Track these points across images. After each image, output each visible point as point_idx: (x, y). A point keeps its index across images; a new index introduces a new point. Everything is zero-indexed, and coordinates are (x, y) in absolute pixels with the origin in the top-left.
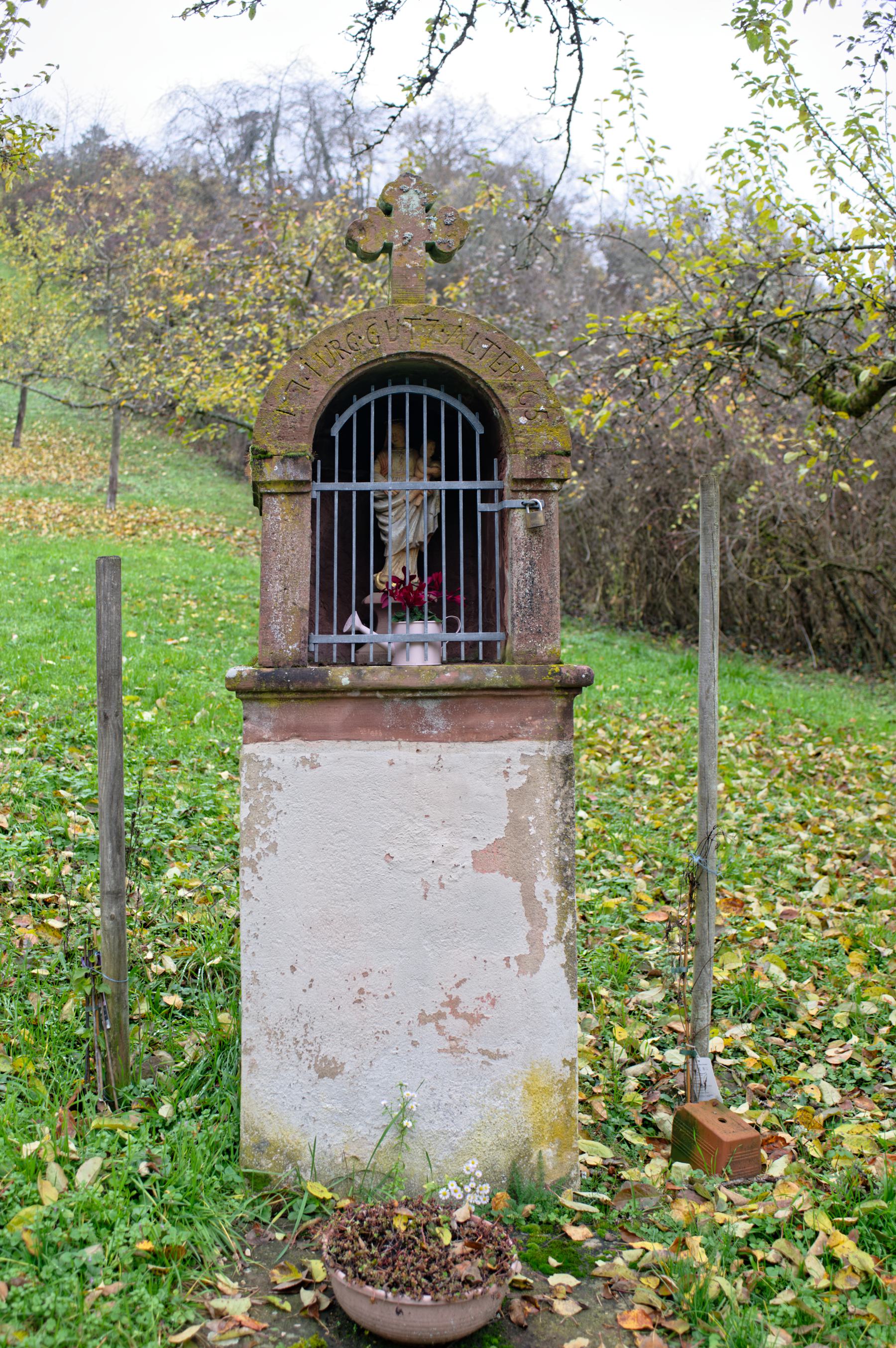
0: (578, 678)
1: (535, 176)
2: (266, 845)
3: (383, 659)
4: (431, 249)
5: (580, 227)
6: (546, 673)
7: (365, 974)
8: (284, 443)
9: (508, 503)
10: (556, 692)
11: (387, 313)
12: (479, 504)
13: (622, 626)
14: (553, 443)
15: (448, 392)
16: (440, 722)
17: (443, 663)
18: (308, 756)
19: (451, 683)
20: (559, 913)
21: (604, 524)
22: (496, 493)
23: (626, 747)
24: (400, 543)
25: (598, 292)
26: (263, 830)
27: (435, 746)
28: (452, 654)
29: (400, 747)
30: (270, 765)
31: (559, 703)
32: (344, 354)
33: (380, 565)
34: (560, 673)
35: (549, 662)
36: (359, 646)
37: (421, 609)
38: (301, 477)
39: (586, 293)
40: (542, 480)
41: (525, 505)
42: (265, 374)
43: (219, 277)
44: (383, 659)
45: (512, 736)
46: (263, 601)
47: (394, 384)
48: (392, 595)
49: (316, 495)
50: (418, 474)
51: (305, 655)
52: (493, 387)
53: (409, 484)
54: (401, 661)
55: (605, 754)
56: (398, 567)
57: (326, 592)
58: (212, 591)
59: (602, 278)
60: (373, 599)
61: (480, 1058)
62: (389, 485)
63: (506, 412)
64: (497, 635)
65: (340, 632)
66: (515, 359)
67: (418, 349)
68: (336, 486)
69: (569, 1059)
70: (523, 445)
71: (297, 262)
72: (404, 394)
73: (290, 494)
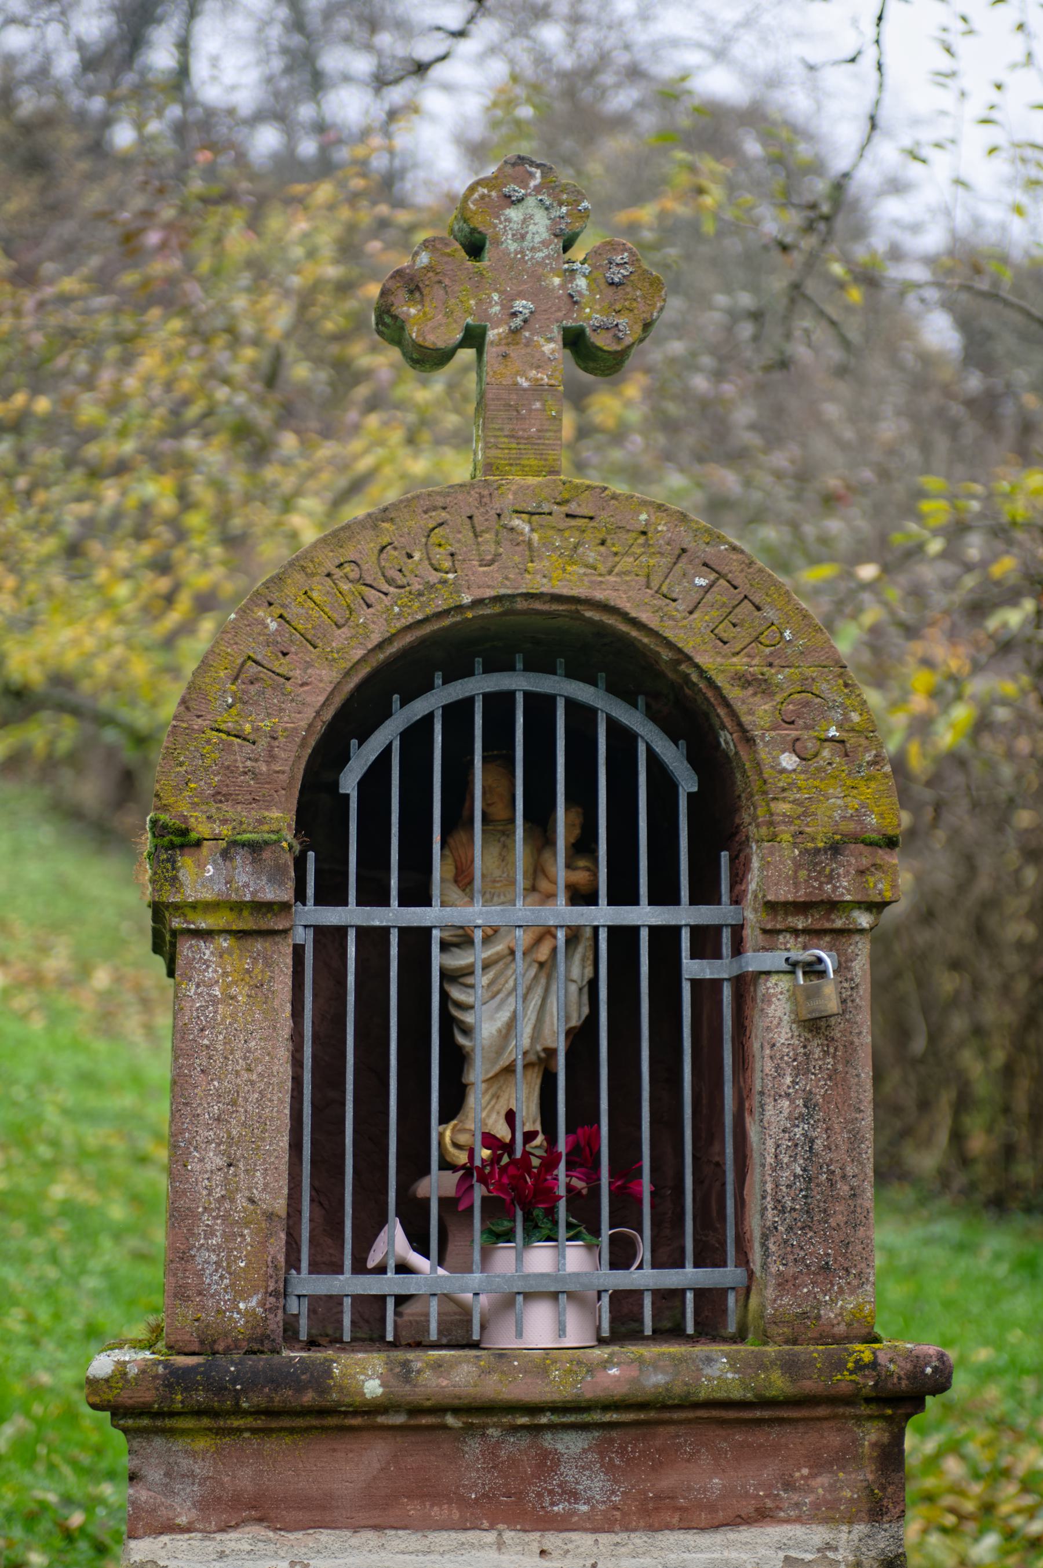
0: (915, 1374)
1: (799, 132)
3: (461, 1333)
4: (575, 341)
5: (896, 254)
6: (839, 1365)
8: (229, 810)
9: (754, 961)
10: (865, 1410)
11: (472, 498)
12: (686, 960)
13: (999, 1204)
14: (858, 816)
15: (615, 689)
16: (595, 1485)
17: (601, 1341)
19: (620, 1391)
21: (956, 965)
22: (726, 935)
23: (1009, 1498)
24: (500, 1050)
25: (940, 412)
27: (583, 1540)
28: (623, 1321)
29: (500, 1545)
31: (872, 1434)
32: (371, 595)
33: (454, 1103)
34: (874, 1364)
35: (848, 1339)
36: (401, 1300)
37: (551, 1213)
38: (270, 894)
39: (912, 415)
40: (833, 906)
41: (793, 965)
42: (169, 599)
43: (61, 361)
44: (461, 1333)
45: (762, 1516)
46: (176, 1194)
47: (487, 670)
48: (483, 1180)
49: (303, 936)
50: (544, 885)
51: (275, 1324)
52: (720, 680)
53: (524, 910)
54: (504, 1338)
55: (962, 1517)
56: (496, 1109)
57: (327, 1164)
58: (38, 1119)
59: (946, 374)
60: (437, 1185)
62: (475, 913)
63: (749, 740)
64: (728, 1275)
65: (360, 1267)
66: (770, 613)
67: (546, 587)
68: (352, 915)
70: (789, 820)
71: (247, 328)
72: (511, 695)
73: (241, 935)
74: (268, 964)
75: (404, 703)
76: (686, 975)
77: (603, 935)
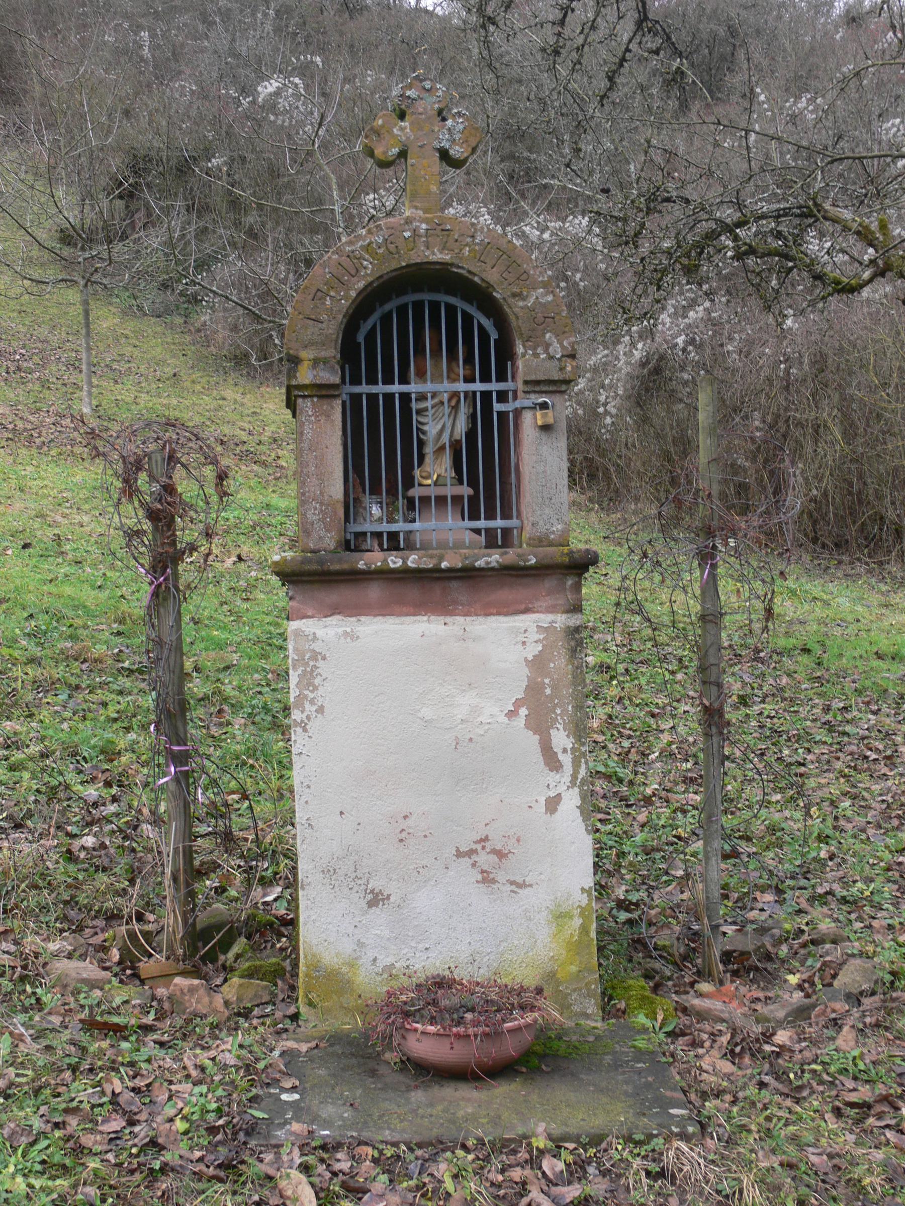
2: (314, 708)
7: (405, 817)
12: (495, 404)
18: (349, 630)
20: (573, 762)
22: (510, 394)
26: (311, 696)
29: (429, 621)
30: (315, 638)
50: (453, 376)
61: (509, 888)
62: (428, 387)
69: (586, 887)
73: (321, 397)
74: (333, 408)
75: (381, 306)
76: (495, 409)
77: (478, 394)
